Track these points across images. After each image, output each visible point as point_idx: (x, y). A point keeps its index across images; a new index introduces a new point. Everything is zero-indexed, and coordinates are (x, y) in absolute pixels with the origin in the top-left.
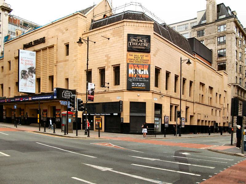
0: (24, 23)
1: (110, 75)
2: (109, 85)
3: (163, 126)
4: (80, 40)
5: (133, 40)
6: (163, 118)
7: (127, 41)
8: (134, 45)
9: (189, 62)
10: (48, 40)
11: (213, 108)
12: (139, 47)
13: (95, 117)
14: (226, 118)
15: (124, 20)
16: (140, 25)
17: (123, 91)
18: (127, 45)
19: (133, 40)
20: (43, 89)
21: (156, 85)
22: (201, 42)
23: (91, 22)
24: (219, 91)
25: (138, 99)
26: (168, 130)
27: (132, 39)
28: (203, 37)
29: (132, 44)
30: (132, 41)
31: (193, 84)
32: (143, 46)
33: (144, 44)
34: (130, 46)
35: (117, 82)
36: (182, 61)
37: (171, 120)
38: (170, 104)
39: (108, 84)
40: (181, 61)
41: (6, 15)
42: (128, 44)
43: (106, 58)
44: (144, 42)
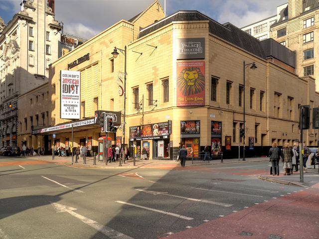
1: (158, 90)
2: (158, 103)
3: (223, 148)
6: (223, 139)
9: (254, 66)
10: (93, 56)
11: (294, 123)
13: (142, 141)
14: (314, 135)
15: (173, 22)
21: (214, 98)
22: (282, 44)
23: (138, 30)
24: (302, 102)
25: (190, 118)
26: (230, 153)
28: (285, 36)
31: (264, 94)
35: (166, 99)
36: (246, 66)
37: (234, 141)
39: (156, 101)
40: (244, 65)
43: (154, 71)
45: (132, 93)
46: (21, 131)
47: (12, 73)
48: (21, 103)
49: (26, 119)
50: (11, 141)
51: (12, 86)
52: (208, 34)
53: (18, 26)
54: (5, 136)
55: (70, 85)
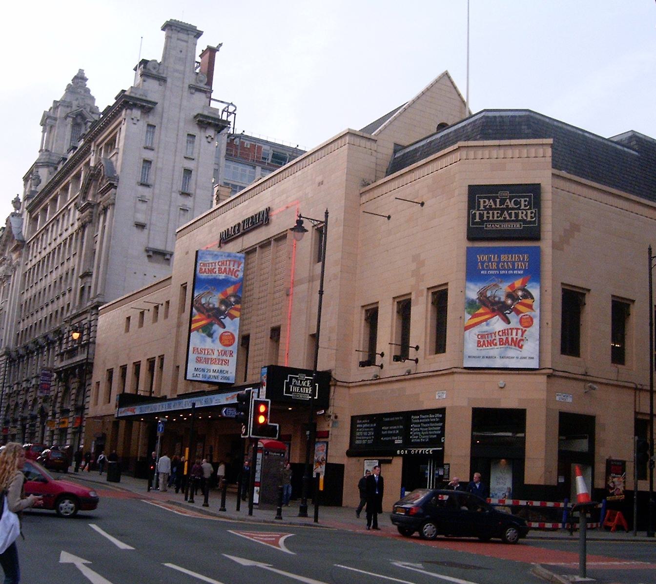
0: (275, 156)
4: (300, 222)
5: (485, 202)
7: (466, 208)
8: (488, 221)
12: (505, 226)
16: (509, 152)
17: (453, 373)
18: (466, 222)
19: (485, 202)
20: (254, 368)
23: (391, 151)
27: (482, 201)
29: (481, 216)
30: (482, 208)
32: (517, 221)
33: (520, 215)
34: (477, 223)
38: (636, 413)
41: (209, 139)
42: (471, 217)
44: (519, 209)
45: (363, 321)
46: (96, 404)
47: (105, 474)
48: (107, 324)
49: (110, 372)
50: (70, 431)
51: (89, 279)
52: (549, 171)
53: (120, 123)
54: (57, 416)
55: (232, 275)
